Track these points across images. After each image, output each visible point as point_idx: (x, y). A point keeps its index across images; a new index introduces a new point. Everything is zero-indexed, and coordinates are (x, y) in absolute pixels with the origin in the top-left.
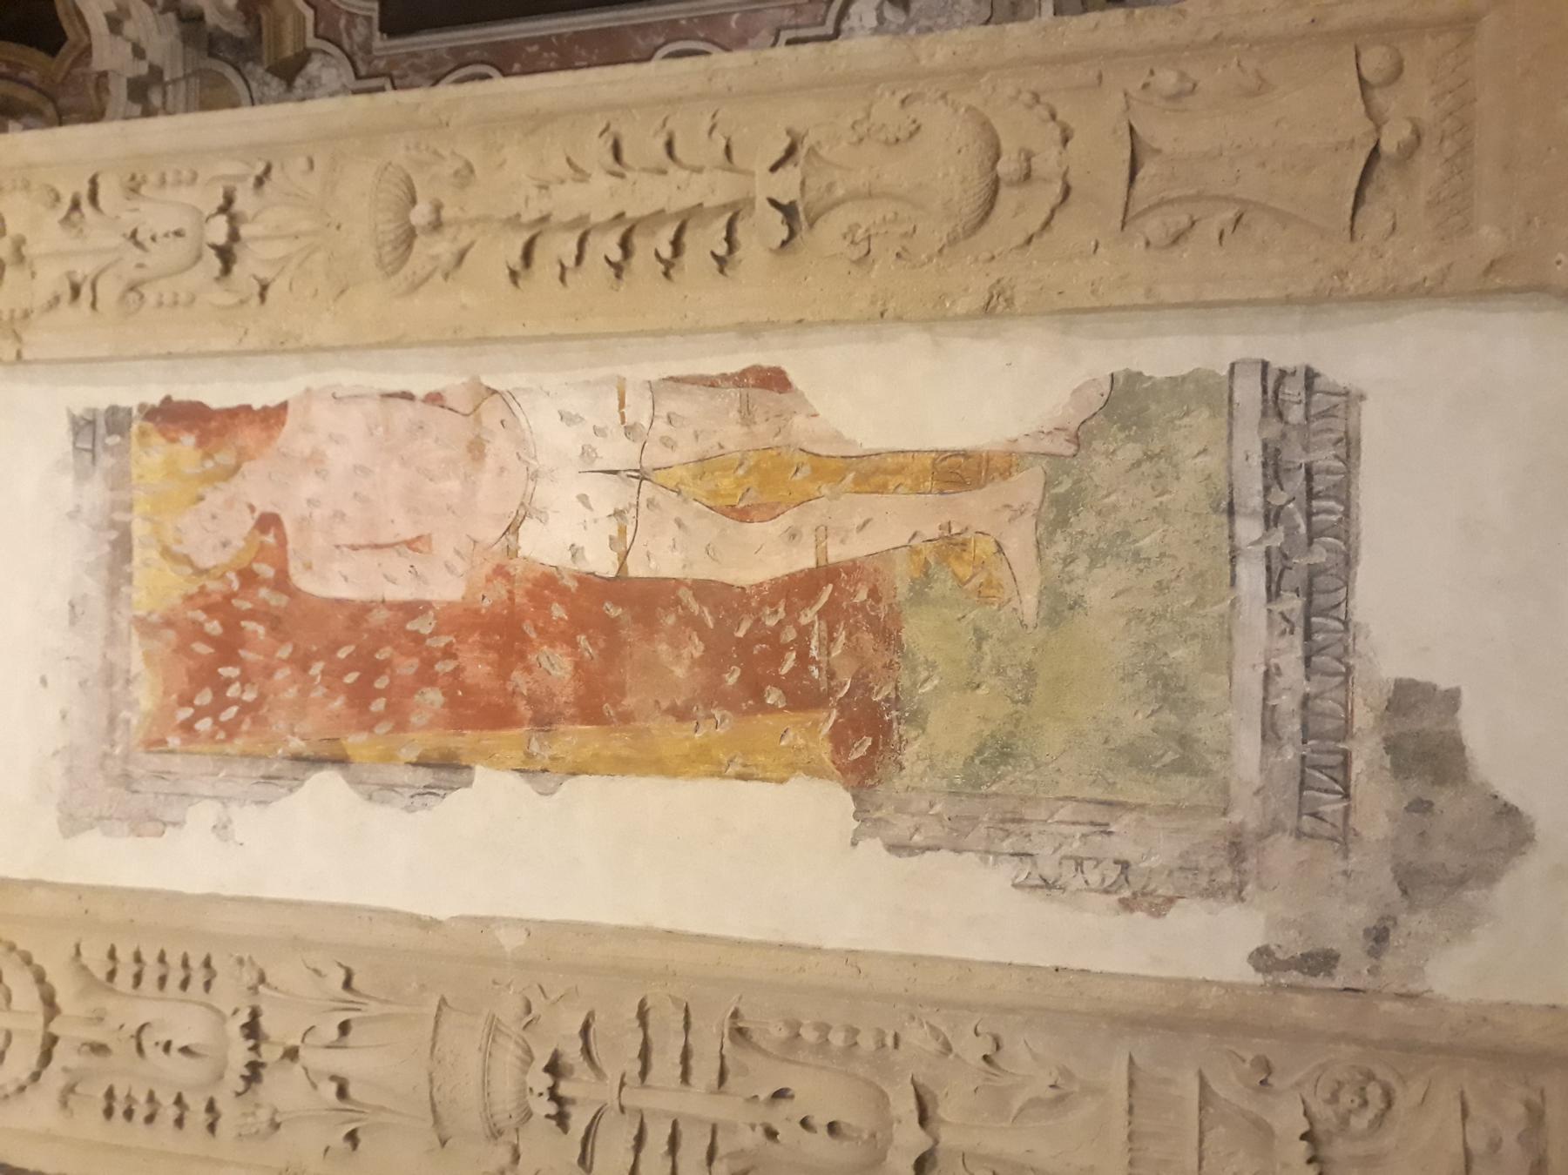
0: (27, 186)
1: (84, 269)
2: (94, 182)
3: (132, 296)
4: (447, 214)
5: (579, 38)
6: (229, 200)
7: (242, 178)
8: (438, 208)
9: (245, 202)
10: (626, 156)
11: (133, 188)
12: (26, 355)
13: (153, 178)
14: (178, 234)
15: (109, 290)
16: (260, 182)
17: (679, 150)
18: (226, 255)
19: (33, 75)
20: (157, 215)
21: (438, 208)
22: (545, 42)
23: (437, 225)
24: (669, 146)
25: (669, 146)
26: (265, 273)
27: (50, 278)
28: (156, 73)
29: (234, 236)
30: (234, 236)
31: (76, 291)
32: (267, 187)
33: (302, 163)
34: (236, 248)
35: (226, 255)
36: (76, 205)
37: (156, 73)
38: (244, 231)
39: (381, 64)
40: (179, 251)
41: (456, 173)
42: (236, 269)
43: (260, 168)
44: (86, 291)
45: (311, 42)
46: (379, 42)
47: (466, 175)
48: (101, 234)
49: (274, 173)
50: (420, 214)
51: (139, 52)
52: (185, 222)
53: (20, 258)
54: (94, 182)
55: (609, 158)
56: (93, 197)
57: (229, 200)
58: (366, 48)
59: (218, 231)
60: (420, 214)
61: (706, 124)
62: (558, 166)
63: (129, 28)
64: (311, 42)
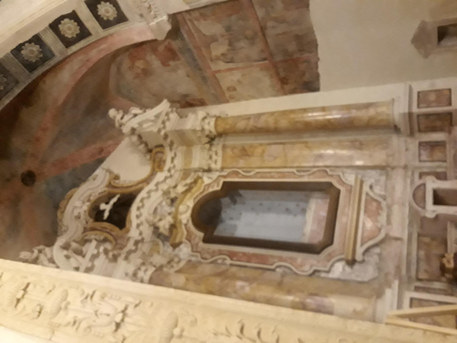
0: (77, 288)
1: (80, 316)
2: (94, 292)
3: (88, 330)
4: (185, 334)
5: (255, 255)
6: (126, 308)
7: (131, 303)
8: (183, 330)
9: (130, 311)
10: (245, 331)
11: (103, 297)
12: (53, 339)
13: (109, 296)
14: (108, 315)
15: (84, 325)
16: (136, 306)
17: (262, 335)
18: (118, 326)
19: (113, 233)
20: (105, 308)
21: (183, 330)
22: (244, 254)
23: (181, 336)
24: (259, 333)
25: (259, 333)
26: (126, 335)
27: (70, 317)
28: (143, 240)
29: (123, 320)
30: (123, 320)
31: (75, 322)
32: (138, 308)
33: (149, 304)
34: (122, 324)
35: (118, 326)
36: (86, 298)
37: (142, 240)
38: (127, 319)
39: (199, 250)
40: (106, 320)
41: (191, 321)
42: (119, 331)
43: (137, 302)
44: (77, 324)
45: (184, 240)
46: (201, 244)
47: (194, 322)
48: (89, 308)
49: (141, 305)
50: (177, 331)
51: (141, 234)
52: (111, 312)
53: (66, 308)
54: (94, 292)
55: (238, 331)
56: (92, 297)
57: (126, 308)
58: (197, 244)
59: (118, 318)
60: (177, 331)
61: (272, 329)
62: (223, 329)
63: (141, 228)
64: (184, 240)
